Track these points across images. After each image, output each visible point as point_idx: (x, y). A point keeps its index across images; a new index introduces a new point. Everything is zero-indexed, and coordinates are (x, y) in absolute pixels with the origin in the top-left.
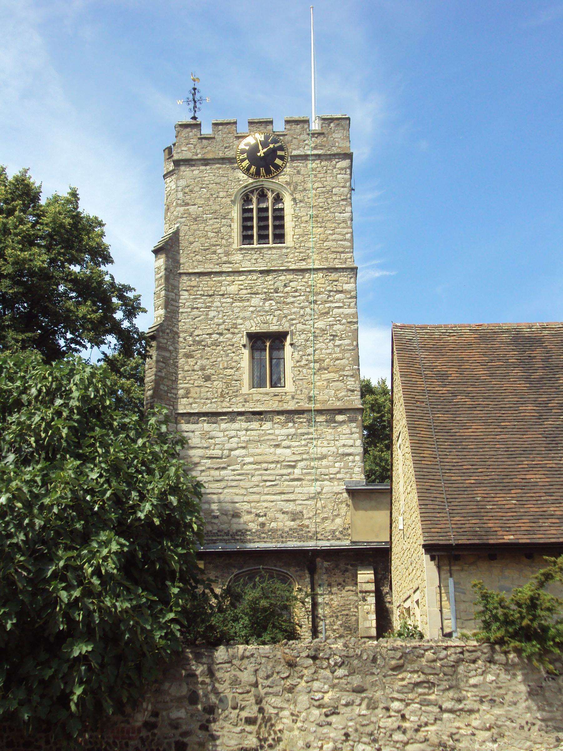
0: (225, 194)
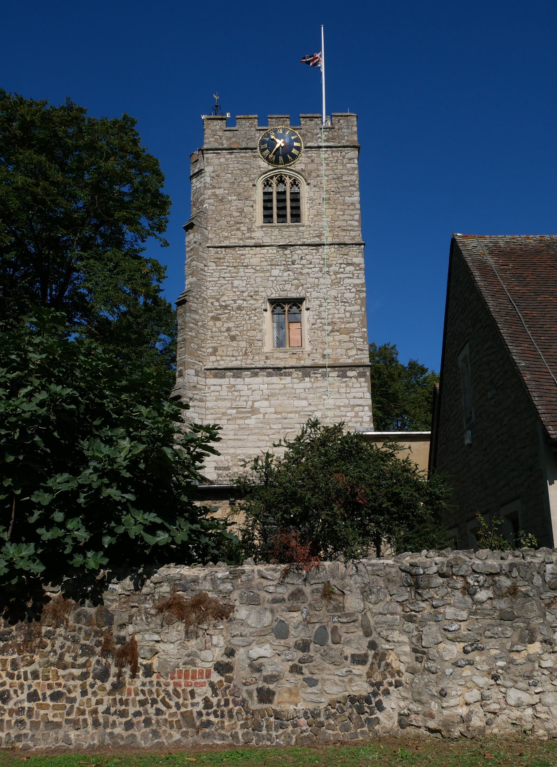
0: (248, 179)
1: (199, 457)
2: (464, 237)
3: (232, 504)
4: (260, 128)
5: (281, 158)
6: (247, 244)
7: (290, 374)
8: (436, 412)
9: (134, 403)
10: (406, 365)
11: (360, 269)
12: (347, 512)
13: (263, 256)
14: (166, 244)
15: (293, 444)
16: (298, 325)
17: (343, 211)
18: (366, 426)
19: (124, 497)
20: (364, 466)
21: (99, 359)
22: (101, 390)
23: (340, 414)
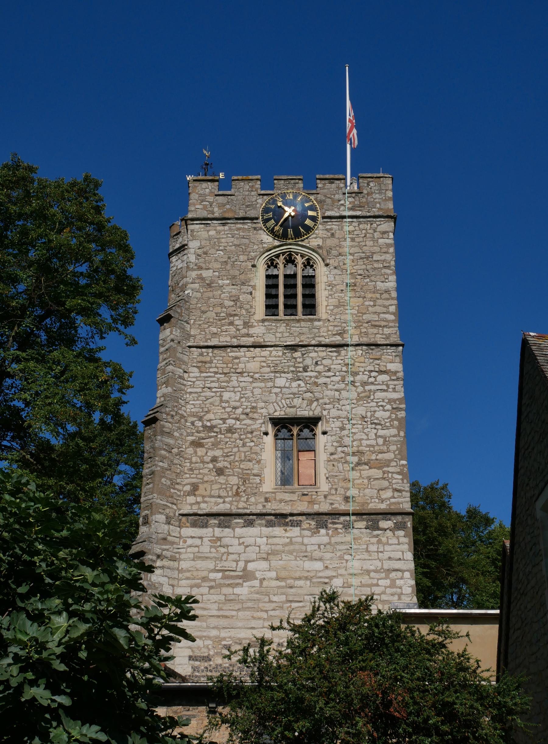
1: (165, 643)
2: (539, 337)
3: (212, 711)
4: (263, 192)
5: (290, 232)
6: (242, 344)
7: (298, 524)
8: (506, 581)
9: (76, 563)
10: (463, 513)
11: (398, 379)
12: (376, 729)
13: (264, 359)
14: (133, 342)
15: (300, 626)
16: (311, 455)
17: (374, 301)
18: (406, 600)
19: (53, 701)
20: (402, 661)
21: (31, 500)
22: (31, 544)
23: (370, 582)
